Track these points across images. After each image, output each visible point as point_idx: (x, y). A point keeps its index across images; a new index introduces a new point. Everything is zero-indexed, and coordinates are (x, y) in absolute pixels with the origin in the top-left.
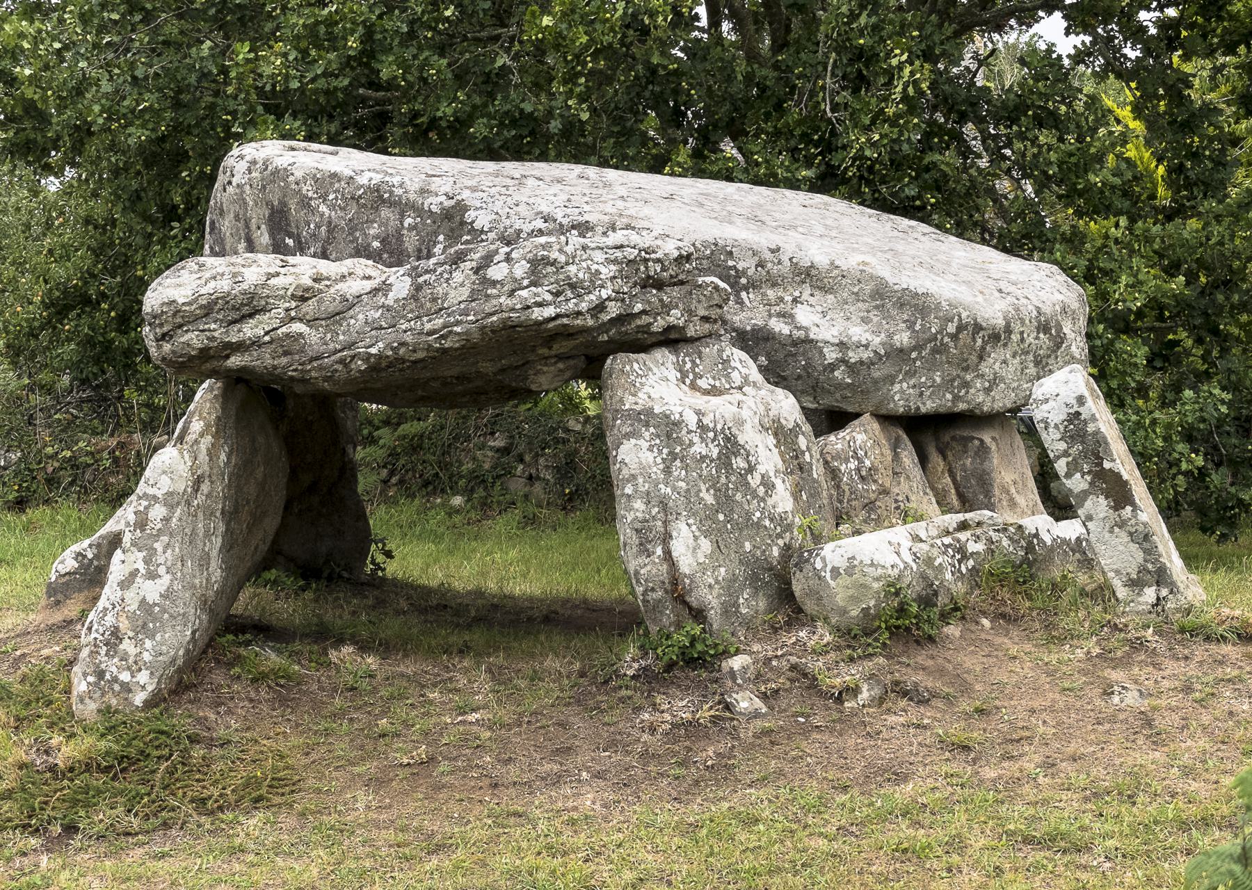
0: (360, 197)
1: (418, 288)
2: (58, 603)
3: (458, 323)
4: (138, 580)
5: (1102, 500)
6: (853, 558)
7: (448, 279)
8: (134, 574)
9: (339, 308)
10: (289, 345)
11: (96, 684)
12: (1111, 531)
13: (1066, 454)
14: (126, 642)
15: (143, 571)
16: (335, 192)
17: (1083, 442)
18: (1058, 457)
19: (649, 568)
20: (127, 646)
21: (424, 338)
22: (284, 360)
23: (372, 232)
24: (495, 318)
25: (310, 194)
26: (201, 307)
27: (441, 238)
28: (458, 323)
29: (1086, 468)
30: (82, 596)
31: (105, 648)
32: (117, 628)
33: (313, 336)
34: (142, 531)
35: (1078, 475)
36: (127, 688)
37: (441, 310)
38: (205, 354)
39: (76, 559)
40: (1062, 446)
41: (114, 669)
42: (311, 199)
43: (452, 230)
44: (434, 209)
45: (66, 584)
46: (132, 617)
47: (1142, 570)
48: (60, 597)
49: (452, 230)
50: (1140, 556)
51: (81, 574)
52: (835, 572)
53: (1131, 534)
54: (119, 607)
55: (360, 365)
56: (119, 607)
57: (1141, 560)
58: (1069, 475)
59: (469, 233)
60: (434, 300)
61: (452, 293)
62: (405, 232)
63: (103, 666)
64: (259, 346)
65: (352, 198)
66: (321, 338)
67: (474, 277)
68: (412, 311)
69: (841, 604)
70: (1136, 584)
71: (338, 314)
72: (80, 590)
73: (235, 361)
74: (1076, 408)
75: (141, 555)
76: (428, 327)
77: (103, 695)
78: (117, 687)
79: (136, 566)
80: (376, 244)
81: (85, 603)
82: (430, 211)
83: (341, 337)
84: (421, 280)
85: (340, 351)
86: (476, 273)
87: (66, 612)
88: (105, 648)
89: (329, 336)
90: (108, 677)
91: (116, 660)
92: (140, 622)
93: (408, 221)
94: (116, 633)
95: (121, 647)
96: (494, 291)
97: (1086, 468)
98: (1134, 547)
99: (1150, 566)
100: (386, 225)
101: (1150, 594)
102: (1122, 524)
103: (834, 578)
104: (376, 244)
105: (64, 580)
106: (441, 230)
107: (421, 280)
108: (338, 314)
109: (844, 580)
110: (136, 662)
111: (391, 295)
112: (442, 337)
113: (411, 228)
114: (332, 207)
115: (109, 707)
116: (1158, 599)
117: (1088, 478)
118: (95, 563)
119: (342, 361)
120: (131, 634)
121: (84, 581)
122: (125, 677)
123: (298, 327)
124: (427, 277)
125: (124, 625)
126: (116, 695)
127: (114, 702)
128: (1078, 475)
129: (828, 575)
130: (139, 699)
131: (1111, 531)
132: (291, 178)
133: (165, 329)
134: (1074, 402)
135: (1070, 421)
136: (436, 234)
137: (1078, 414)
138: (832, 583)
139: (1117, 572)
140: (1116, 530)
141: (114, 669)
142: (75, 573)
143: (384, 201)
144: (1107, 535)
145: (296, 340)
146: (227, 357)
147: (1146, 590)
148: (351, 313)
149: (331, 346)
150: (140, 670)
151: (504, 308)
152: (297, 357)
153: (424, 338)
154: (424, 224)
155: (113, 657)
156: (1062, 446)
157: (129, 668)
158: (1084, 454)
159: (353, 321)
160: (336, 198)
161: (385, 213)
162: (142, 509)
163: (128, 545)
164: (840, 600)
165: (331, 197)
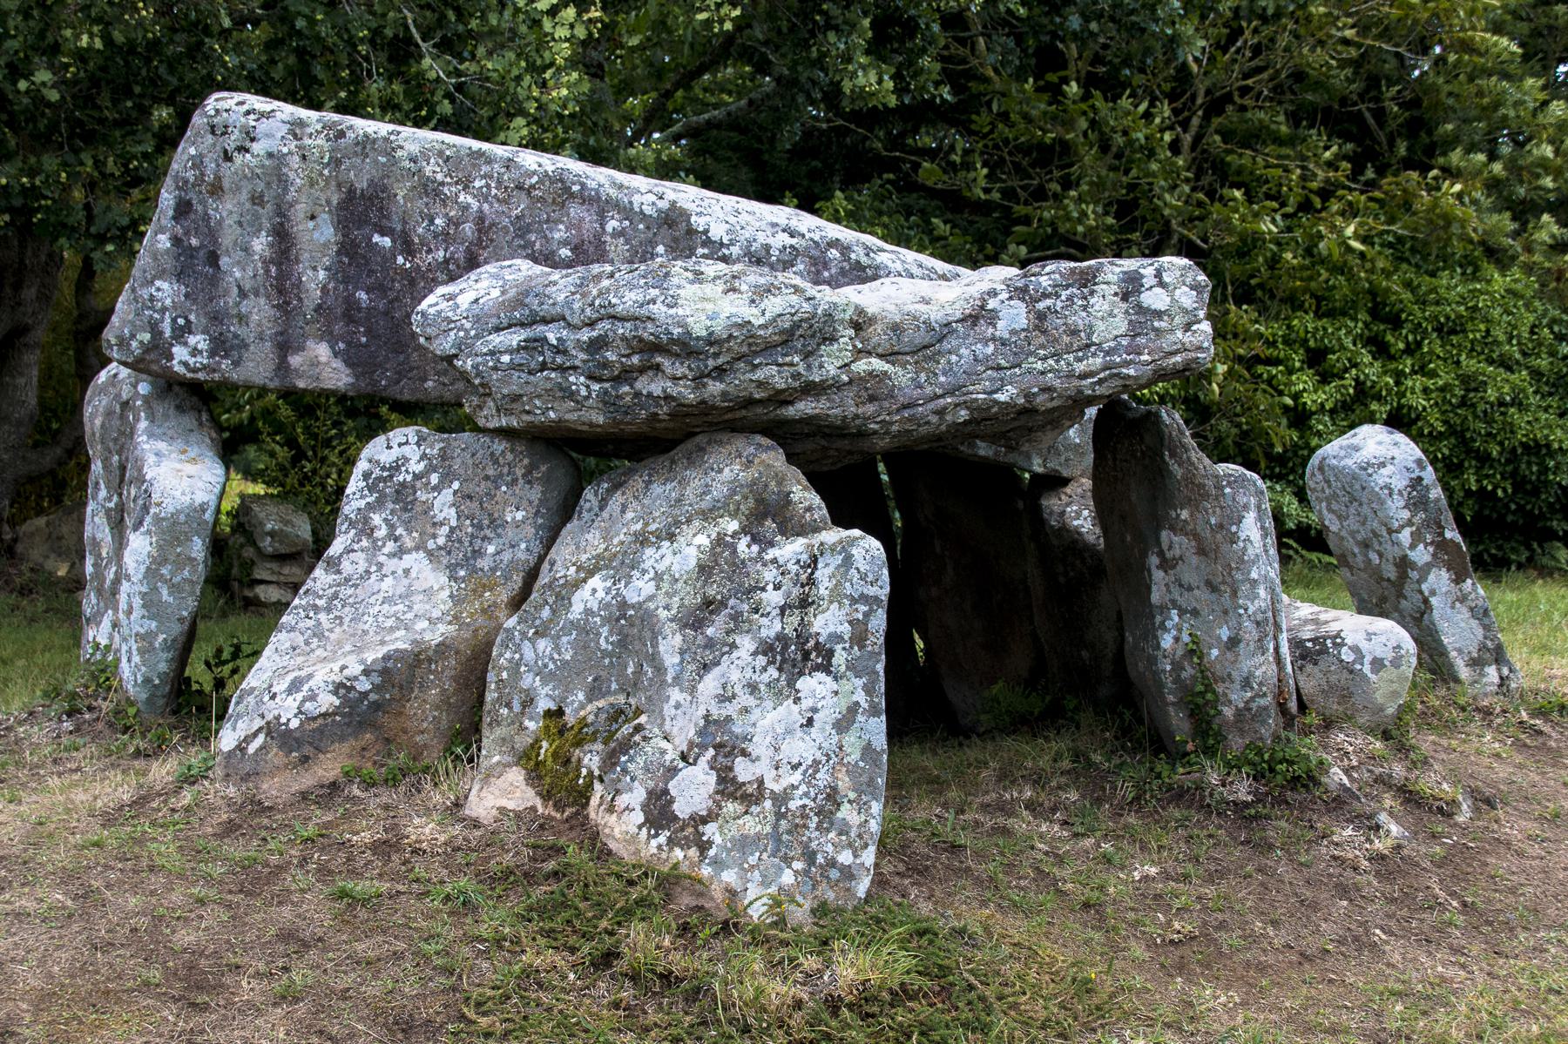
0: (533, 187)
1: (1041, 316)
2: (305, 760)
3: (1127, 364)
4: (860, 718)
5: (1444, 574)
6: (1399, 647)
7: (1085, 308)
8: (853, 709)
9: (927, 340)
10: (872, 388)
11: (806, 872)
12: (1453, 607)
13: (1410, 523)
14: (846, 807)
15: (865, 705)
16: (483, 177)
17: (1425, 510)
18: (1403, 527)
19: (1264, 668)
20: (847, 813)
21: (1076, 383)
22: (870, 409)
23: (557, 236)
24: (1178, 358)
25: (439, 177)
26: (782, 332)
27: (660, 249)
28: (1127, 364)
29: (1429, 538)
30: (345, 747)
31: (815, 819)
32: (834, 789)
33: (901, 376)
34: (862, 647)
35: (1421, 546)
36: (848, 873)
37: (1088, 346)
38: (781, 398)
39: (335, 693)
40: (1406, 514)
41: (829, 849)
42: (442, 184)
43: (675, 240)
44: (648, 210)
45: (320, 731)
46: (852, 771)
47: (1483, 648)
48: (308, 750)
49: (675, 240)
50: (1480, 632)
51: (343, 715)
52: (1378, 664)
53: (1472, 609)
54: (834, 759)
55: (963, 414)
56: (834, 759)
57: (1481, 638)
58: (1413, 547)
59: (704, 245)
60: (1074, 333)
61: (1100, 326)
62: (608, 239)
63: (814, 845)
64: (838, 388)
65: (519, 187)
66: (913, 380)
67: (1125, 305)
68: (1042, 347)
69: (1380, 700)
70: (1476, 663)
71: (926, 347)
72: (342, 739)
73: (805, 407)
74: (1417, 473)
75: (859, 682)
76: (1080, 367)
77: (814, 887)
78: (834, 874)
79: (855, 698)
80: (565, 252)
81: (350, 756)
82: (642, 212)
83: (942, 379)
84: (1041, 306)
85: (942, 396)
86: (1125, 298)
87: (321, 772)
88: (815, 819)
89: (923, 377)
90: (820, 859)
91: (832, 835)
92: (864, 779)
93: (612, 225)
94: (833, 796)
95: (839, 815)
96: (1163, 324)
97: (1429, 538)
98: (1474, 623)
99: (1489, 644)
100: (579, 228)
101: (1492, 673)
102: (1463, 599)
103: (1375, 671)
104: (565, 252)
105: (314, 725)
106: (659, 238)
107: (1041, 306)
108: (926, 347)
109: (1389, 673)
110: (860, 836)
111: (1000, 324)
112: (1101, 382)
113: (617, 234)
114: (483, 197)
115: (824, 904)
116: (1501, 678)
117: (1431, 549)
118: (373, 697)
119: (941, 412)
120: (852, 795)
121: (348, 724)
122: (845, 858)
123: (878, 364)
124: (1049, 302)
125: (844, 783)
126: (833, 885)
127: (830, 895)
128: (1421, 546)
129: (1367, 669)
130: (862, 887)
131: (1453, 607)
132: (399, 153)
133: (720, 361)
134: (1414, 466)
135: (1413, 487)
136: (653, 244)
137: (1420, 479)
138: (1373, 677)
139: (1460, 651)
140: (1458, 605)
141: (829, 849)
142: (334, 714)
143: (572, 195)
144: (1449, 611)
145: (881, 381)
146: (791, 403)
147: (1487, 669)
148: (946, 345)
149: (928, 390)
150: (866, 846)
151: (1188, 346)
152: (886, 404)
153: (1076, 383)
154: (636, 230)
155: (828, 830)
156: (1406, 514)
157: (850, 845)
158: (1427, 524)
159: (954, 358)
160: (488, 186)
161: (575, 210)
162: (860, 617)
163: (843, 668)
164: (1379, 697)
165: (477, 184)
